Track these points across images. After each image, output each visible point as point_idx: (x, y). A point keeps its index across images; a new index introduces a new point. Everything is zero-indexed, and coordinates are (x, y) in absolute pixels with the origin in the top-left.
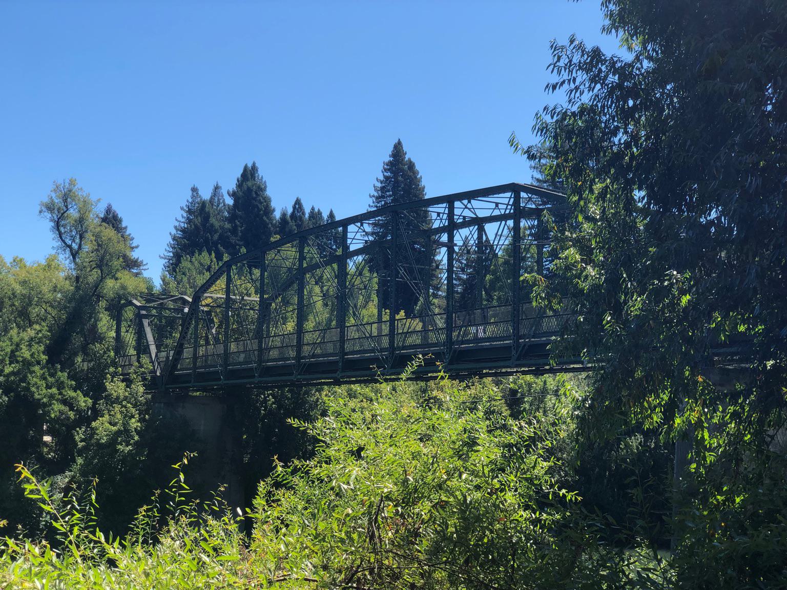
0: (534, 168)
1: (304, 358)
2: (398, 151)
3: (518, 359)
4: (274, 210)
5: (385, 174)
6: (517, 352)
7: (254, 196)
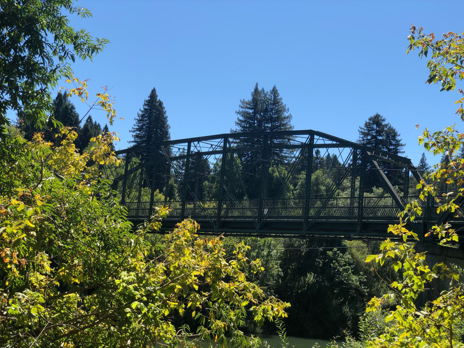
0: (238, 113)
2: (153, 95)
3: (307, 230)
5: (145, 107)
6: (307, 226)
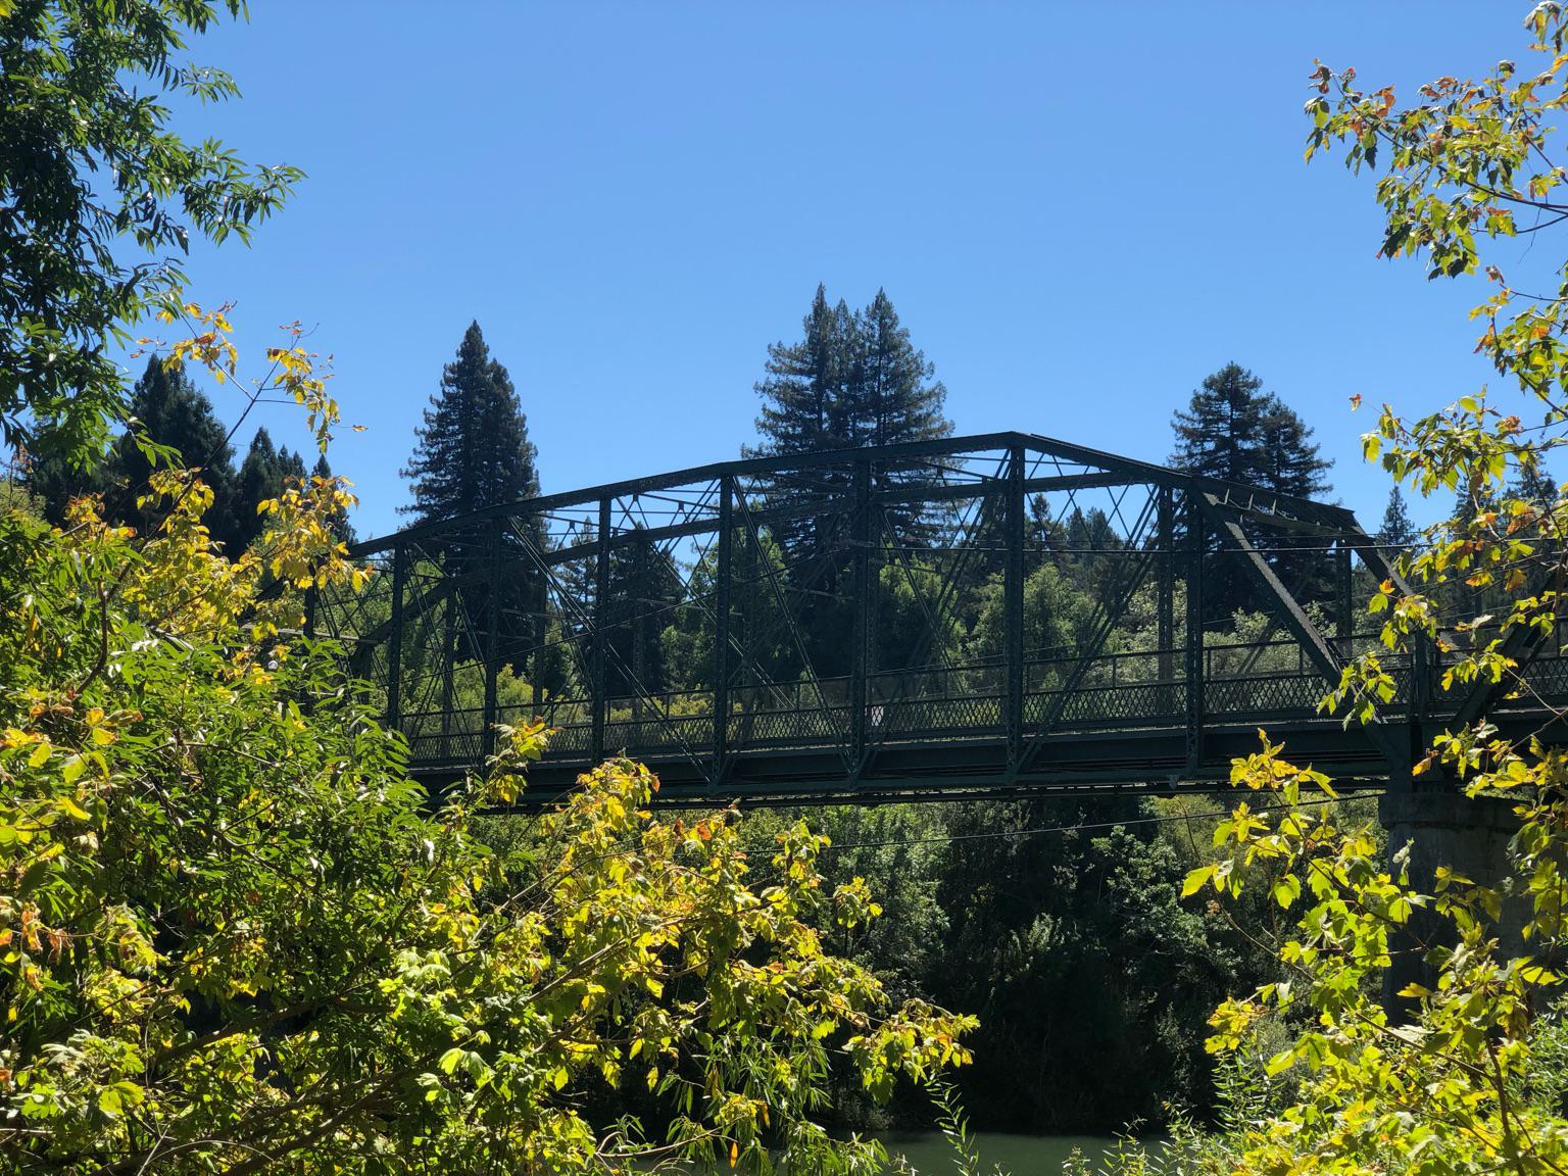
0: (764, 390)
1: (730, 746)
2: (473, 345)
3: (1021, 771)
4: (233, 452)
5: (447, 389)
7: (193, 420)
